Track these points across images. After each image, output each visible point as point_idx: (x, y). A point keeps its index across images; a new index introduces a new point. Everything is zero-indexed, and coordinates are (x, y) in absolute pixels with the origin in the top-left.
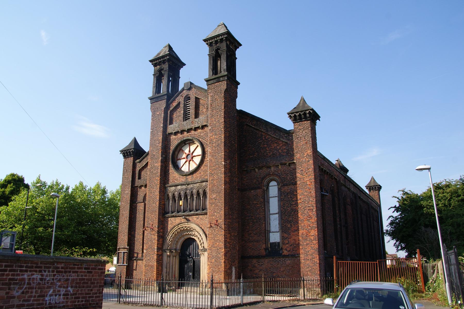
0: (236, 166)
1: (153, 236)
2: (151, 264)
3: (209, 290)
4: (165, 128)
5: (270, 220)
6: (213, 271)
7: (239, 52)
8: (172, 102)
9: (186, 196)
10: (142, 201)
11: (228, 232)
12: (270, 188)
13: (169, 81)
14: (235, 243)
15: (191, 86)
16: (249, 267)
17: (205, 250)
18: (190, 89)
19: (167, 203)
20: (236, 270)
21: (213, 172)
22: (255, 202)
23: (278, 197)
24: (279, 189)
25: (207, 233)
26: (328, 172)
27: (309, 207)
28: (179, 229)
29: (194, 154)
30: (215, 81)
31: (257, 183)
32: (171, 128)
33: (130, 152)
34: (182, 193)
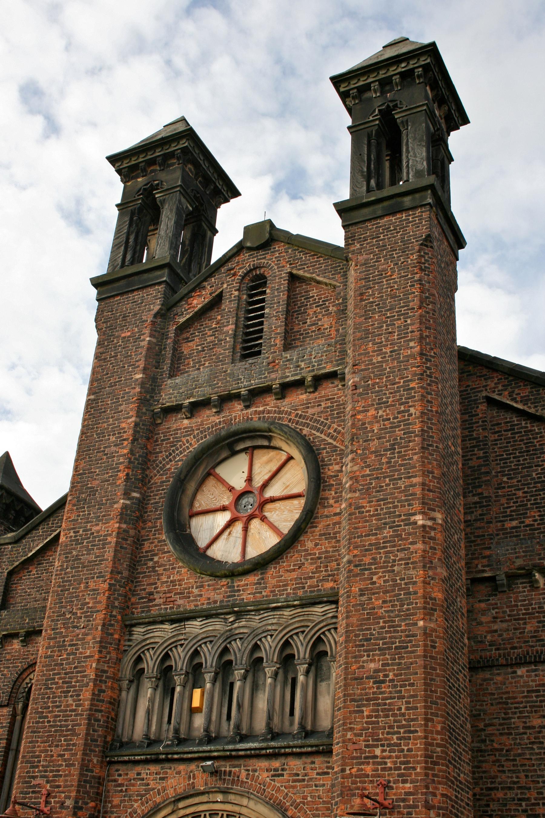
4: (151, 387)
8: (187, 296)
9: (225, 668)
15: (264, 237)
18: (265, 246)
19: (127, 697)
21: (367, 560)
29: (270, 493)
30: (379, 209)
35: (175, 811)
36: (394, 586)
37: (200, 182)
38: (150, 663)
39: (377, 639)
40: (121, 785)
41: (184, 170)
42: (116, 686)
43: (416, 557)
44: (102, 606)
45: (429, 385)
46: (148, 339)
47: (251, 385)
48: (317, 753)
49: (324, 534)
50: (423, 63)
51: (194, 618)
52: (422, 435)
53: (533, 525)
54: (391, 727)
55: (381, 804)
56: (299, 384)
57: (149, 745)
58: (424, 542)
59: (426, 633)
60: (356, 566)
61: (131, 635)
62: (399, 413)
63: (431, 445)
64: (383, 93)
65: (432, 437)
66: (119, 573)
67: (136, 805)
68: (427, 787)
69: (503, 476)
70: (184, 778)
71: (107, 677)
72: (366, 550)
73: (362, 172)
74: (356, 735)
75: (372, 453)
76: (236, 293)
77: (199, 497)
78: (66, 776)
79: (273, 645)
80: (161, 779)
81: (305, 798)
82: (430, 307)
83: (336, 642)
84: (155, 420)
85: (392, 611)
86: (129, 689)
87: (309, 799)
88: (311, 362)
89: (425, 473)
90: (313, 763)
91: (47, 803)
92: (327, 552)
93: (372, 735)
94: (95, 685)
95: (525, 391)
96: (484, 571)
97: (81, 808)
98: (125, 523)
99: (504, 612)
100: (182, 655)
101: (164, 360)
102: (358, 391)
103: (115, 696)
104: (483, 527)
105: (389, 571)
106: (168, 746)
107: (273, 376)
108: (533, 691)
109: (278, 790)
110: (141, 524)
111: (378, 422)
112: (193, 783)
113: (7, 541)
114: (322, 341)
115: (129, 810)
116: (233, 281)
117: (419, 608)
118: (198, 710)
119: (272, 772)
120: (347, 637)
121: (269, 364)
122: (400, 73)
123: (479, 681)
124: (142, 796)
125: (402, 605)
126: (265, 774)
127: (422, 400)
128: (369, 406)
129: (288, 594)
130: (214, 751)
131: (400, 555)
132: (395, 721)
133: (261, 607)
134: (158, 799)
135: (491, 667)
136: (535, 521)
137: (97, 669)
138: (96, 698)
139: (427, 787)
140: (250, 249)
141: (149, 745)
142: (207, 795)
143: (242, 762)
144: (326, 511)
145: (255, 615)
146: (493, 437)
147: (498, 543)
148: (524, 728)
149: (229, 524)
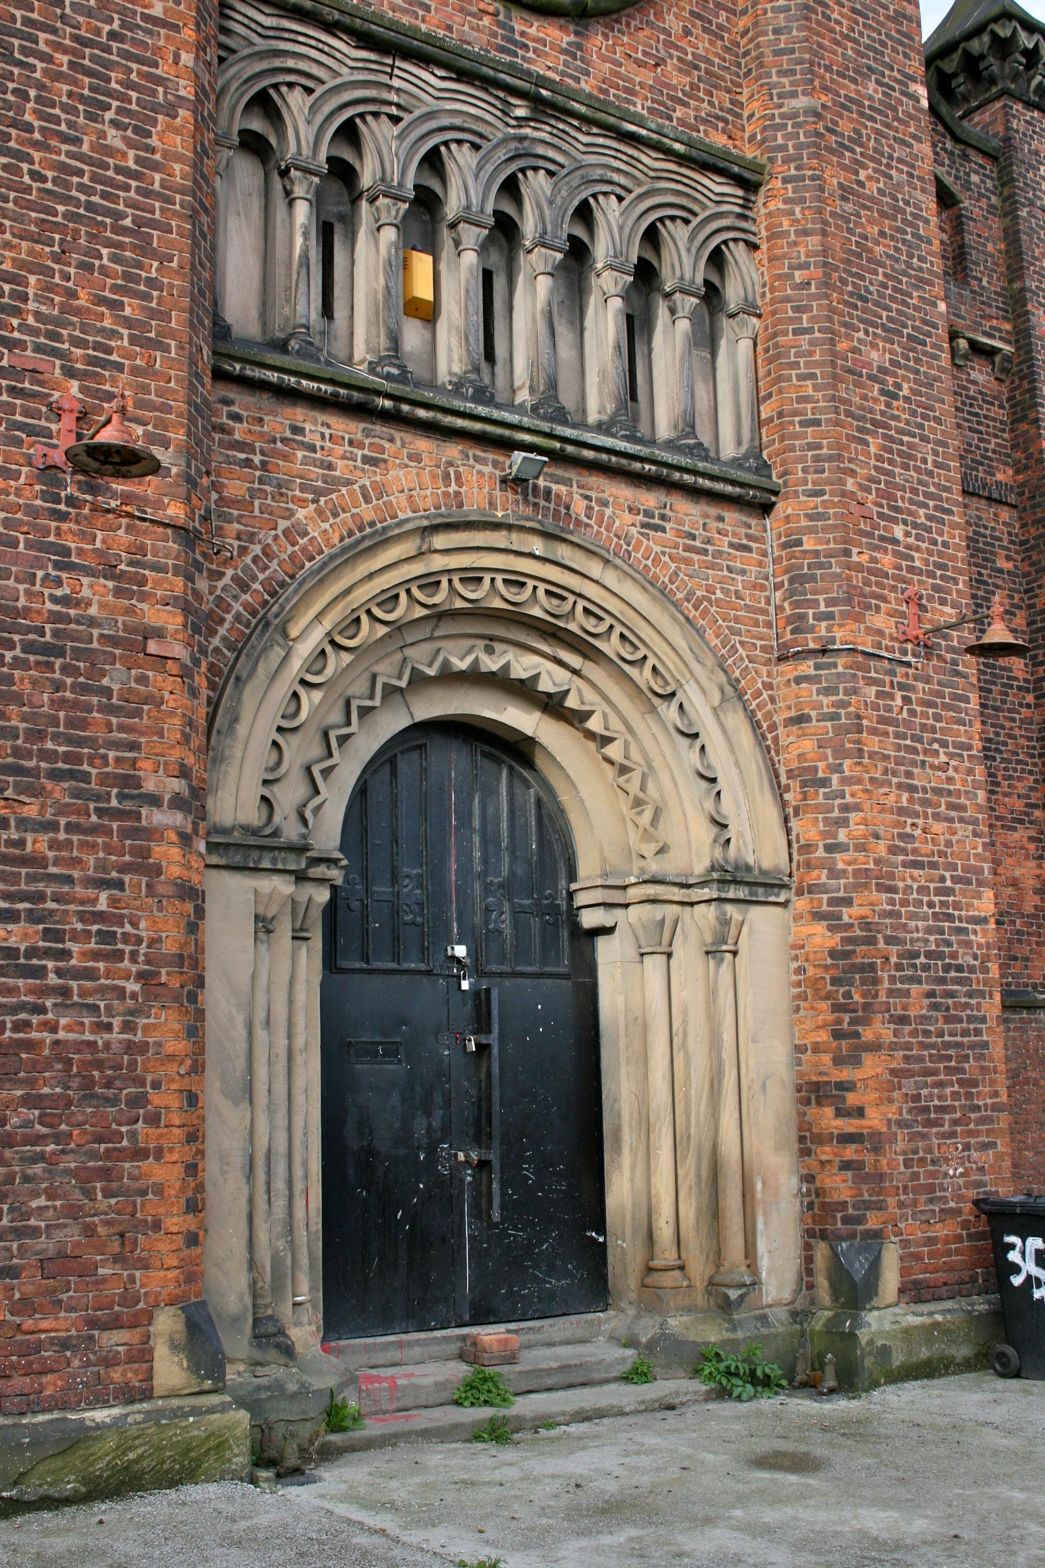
28: (430, 582)
35: (422, 554)
40: (241, 446)
51: (425, 60)
67: (301, 514)
70: (434, 477)
78: (135, 371)
80: (366, 460)
81: (711, 590)
87: (719, 594)
90: (720, 519)
112: (458, 494)
115: (283, 524)
119: (640, 517)
124: (318, 493)
130: (528, 430)
142: (505, 533)
145: (579, 129)
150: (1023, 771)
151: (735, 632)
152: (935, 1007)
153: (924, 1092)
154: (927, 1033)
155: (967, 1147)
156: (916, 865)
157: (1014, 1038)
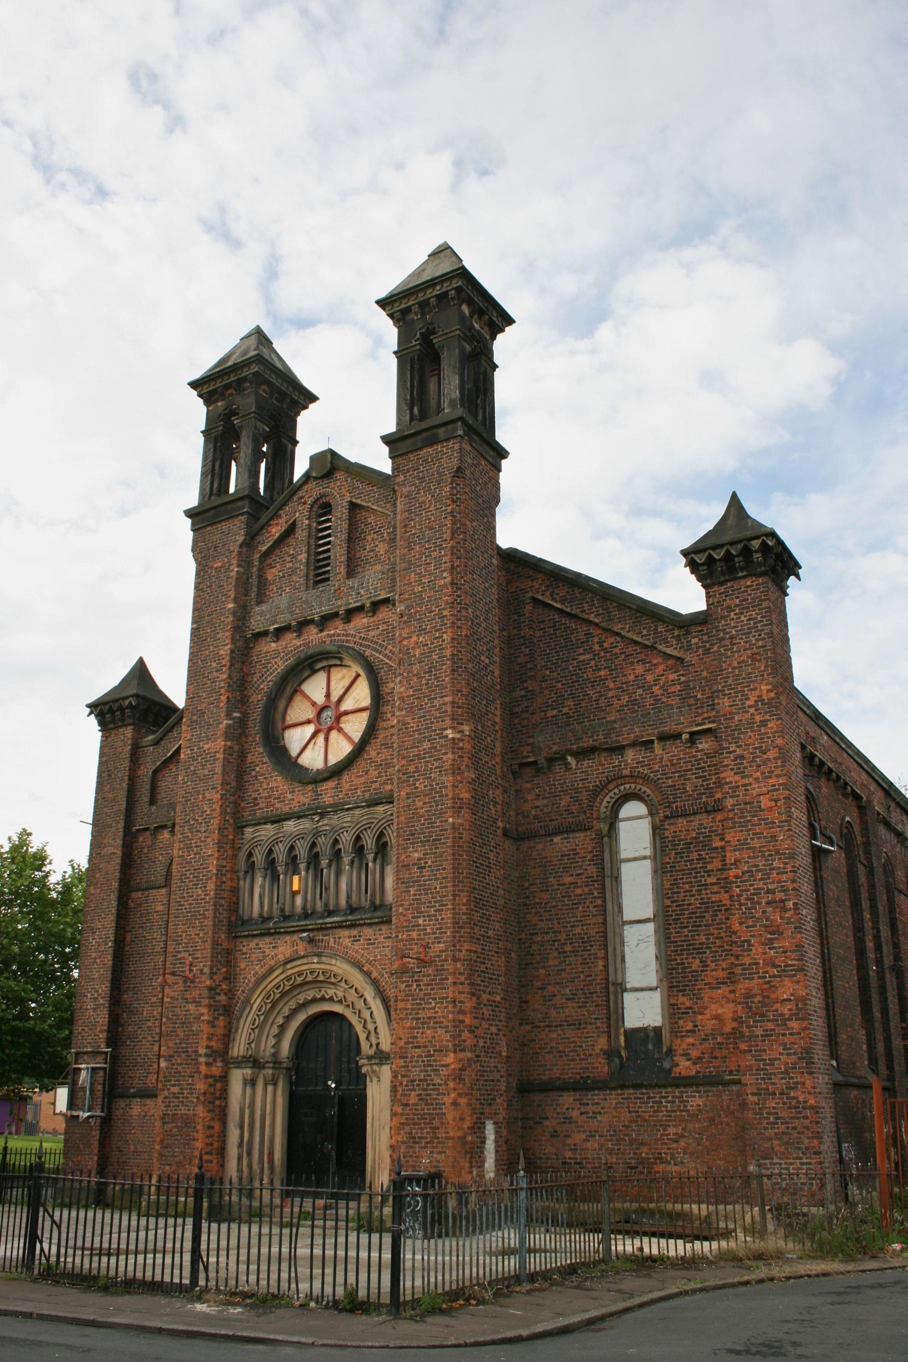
0: (498, 744)
1: (191, 1007)
2: (183, 1110)
3: (191, 1200)
4: (242, 615)
5: (623, 943)
6: (413, 1139)
7: (503, 346)
8: (267, 524)
9: (314, 859)
10: (161, 881)
11: (467, 988)
12: (623, 827)
13: (258, 456)
14: (494, 1029)
15: (329, 464)
16: (546, 1123)
17: (381, 1057)
18: (328, 475)
19: (244, 885)
20: (497, 1133)
22: (567, 880)
23: (654, 858)
24: (656, 830)
25: (390, 993)
26: (830, 771)
27: (769, 891)
28: (288, 979)
31: (574, 809)
32: (262, 617)
33: (121, 709)
34: (302, 850)
36: (431, 790)
37: (276, 399)
38: (259, 858)
39: (419, 834)
41: (257, 393)
42: (234, 877)
43: (447, 765)
44: (216, 814)
45: (459, 612)
46: (236, 569)
47: (322, 611)
48: (383, 922)
49: (384, 744)
50: (455, 286)
52: (453, 659)
53: (568, 713)
54: (430, 902)
55: (423, 960)
56: (361, 609)
57: (263, 922)
58: (453, 753)
59: (454, 828)
60: (403, 774)
61: (243, 834)
62: (435, 639)
63: (461, 667)
64: (423, 314)
65: (461, 659)
66: (228, 784)
68: (454, 946)
69: (546, 669)
71: (227, 871)
72: (411, 760)
73: (406, 400)
74: (405, 909)
75: (414, 675)
76: (307, 522)
77: (289, 711)
79: (349, 839)
81: (376, 956)
82: (461, 537)
83: (392, 836)
84: (248, 644)
85: (430, 811)
86: (245, 878)
88: (369, 590)
89: (454, 693)
90: (381, 930)
91: (191, 971)
92: (386, 759)
93: (417, 908)
94: (217, 878)
95: (562, 592)
96: (528, 757)
97: (216, 973)
98: (230, 740)
99: (545, 791)
100: (282, 850)
101: (253, 587)
102: (403, 619)
103: (235, 885)
104: (528, 718)
105: (427, 778)
106: (276, 922)
107: (339, 603)
108: (565, 855)
109: (357, 952)
110: (244, 739)
111: (419, 647)
113: (148, 744)
114: (378, 567)
116: (304, 509)
117: (449, 808)
118: (298, 892)
120: (398, 833)
121: (335, 591)
122: (436, 296)
123: (525, 849)
124: (261, 961)
125: (437, 806)
126: (348, 940)
127: (452, 627)
128: (412, 633)
129: (358, 796)
131: (436, 764)
132: (433, 898)
133: (338, 808)
134: (272, 963)
135: (535, 837)
136: (571, 709)
137: (217, 865)
138: (219, 888)
139: (454, 946)
140: (316, 478)
141: (263, 922)
143: (330, 931)
144: (385, 724)
146: (539, 634)
147: (541, 731)
148: (558, 885)
149: (314, 735)
150: (726, 955)
151: (383, 969)
152: (421, 1100)
153: (414, 1131)
154: (416, 1110)
155: (432, 1152)
156: (419, 1047)
157: (712, 1101)
